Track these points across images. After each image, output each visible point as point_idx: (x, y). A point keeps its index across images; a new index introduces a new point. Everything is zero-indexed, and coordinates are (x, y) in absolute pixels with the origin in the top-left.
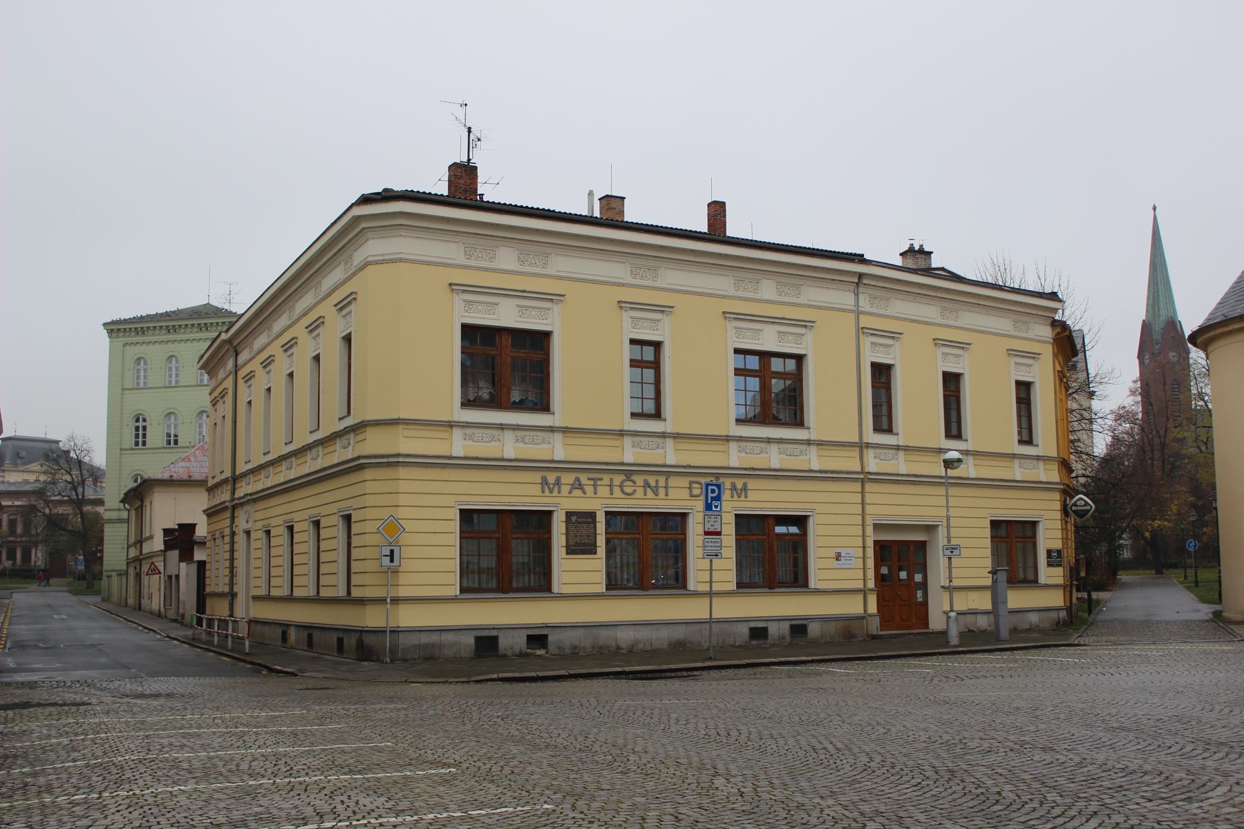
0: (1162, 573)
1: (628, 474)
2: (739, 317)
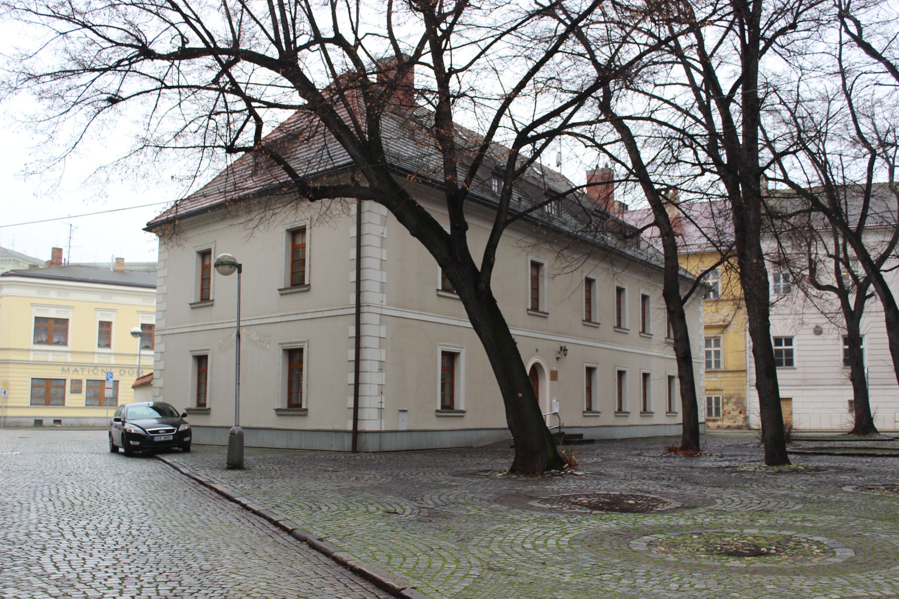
0: (209, 409)
1: (96, 367)
2: (143, 312)
